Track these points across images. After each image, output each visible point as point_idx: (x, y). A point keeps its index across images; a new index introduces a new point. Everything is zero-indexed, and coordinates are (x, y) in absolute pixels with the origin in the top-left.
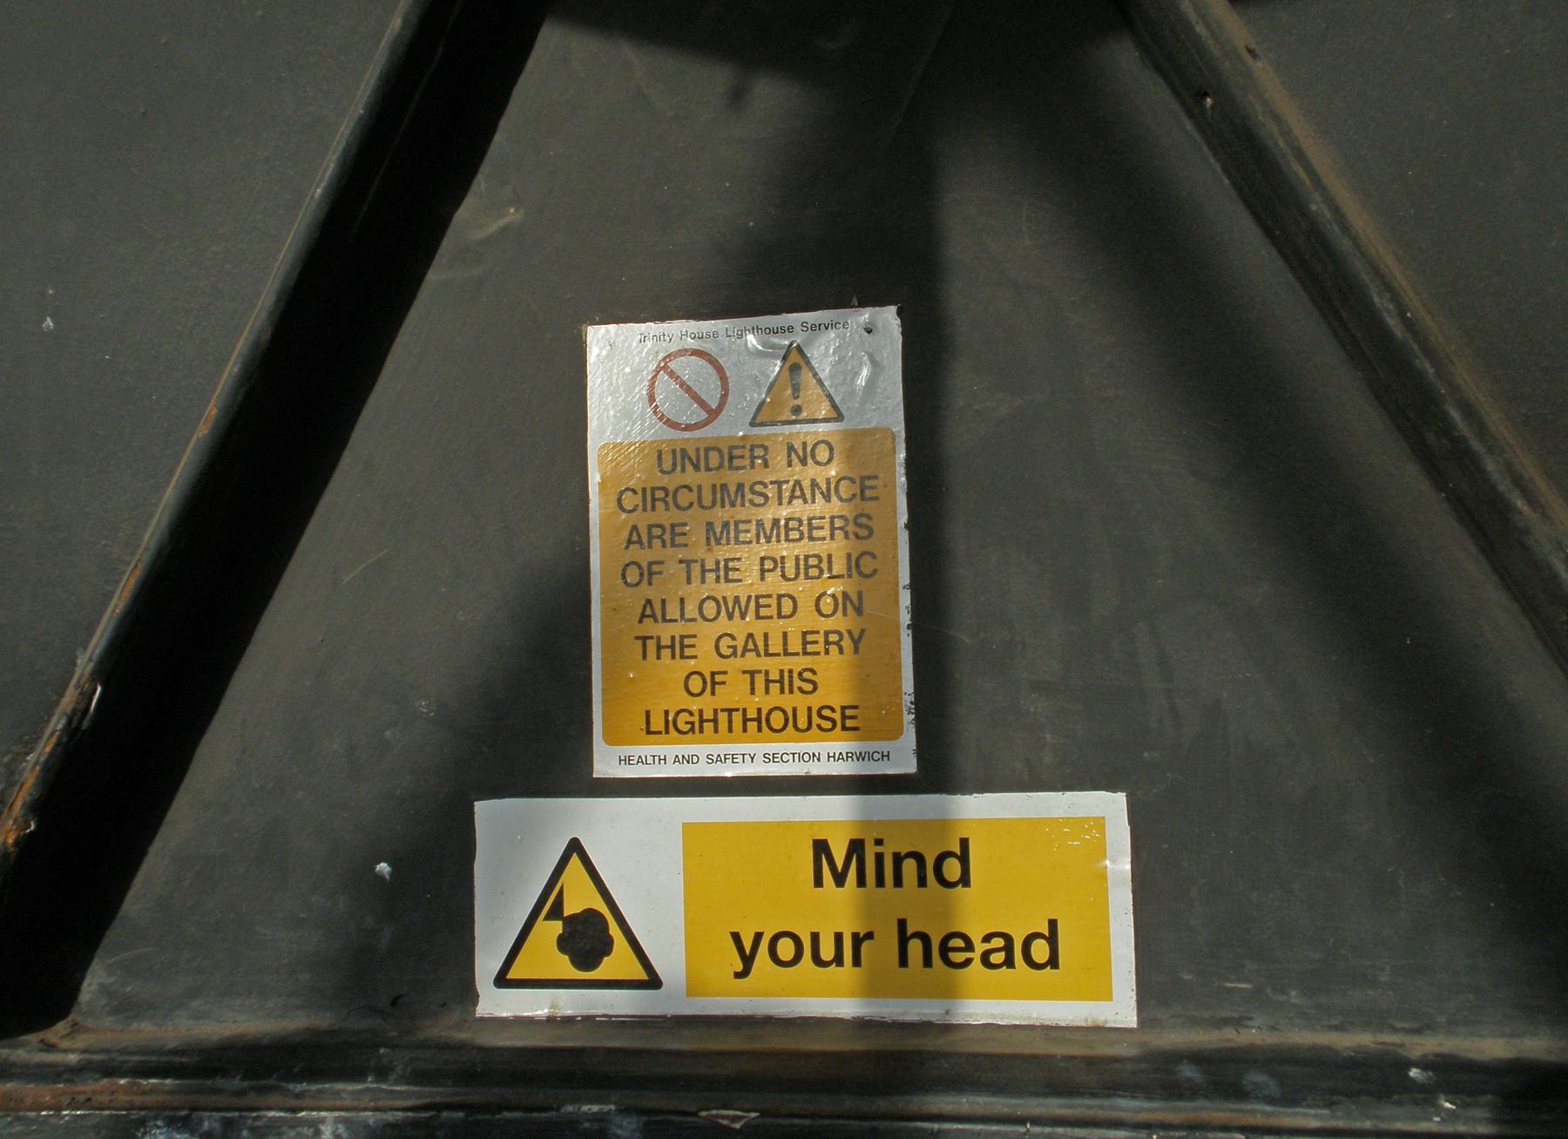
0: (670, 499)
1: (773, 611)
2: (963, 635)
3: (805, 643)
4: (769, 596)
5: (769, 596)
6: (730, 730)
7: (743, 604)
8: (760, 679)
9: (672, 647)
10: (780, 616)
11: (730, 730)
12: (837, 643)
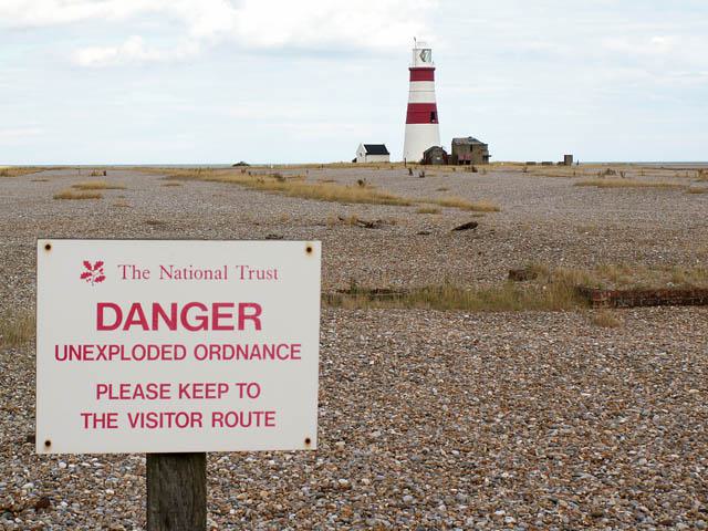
0: (223, 420)
1: (172, 355)
2: (656, 281)
3: (122, 392)
4: (201, 385)
5: (201, 385)
6: (258, 425)
7: (73, 355)
8: (91, 419)
9: (103, 420)
10: (176, 358)
11: (258, 425)
12: (253, 317)
